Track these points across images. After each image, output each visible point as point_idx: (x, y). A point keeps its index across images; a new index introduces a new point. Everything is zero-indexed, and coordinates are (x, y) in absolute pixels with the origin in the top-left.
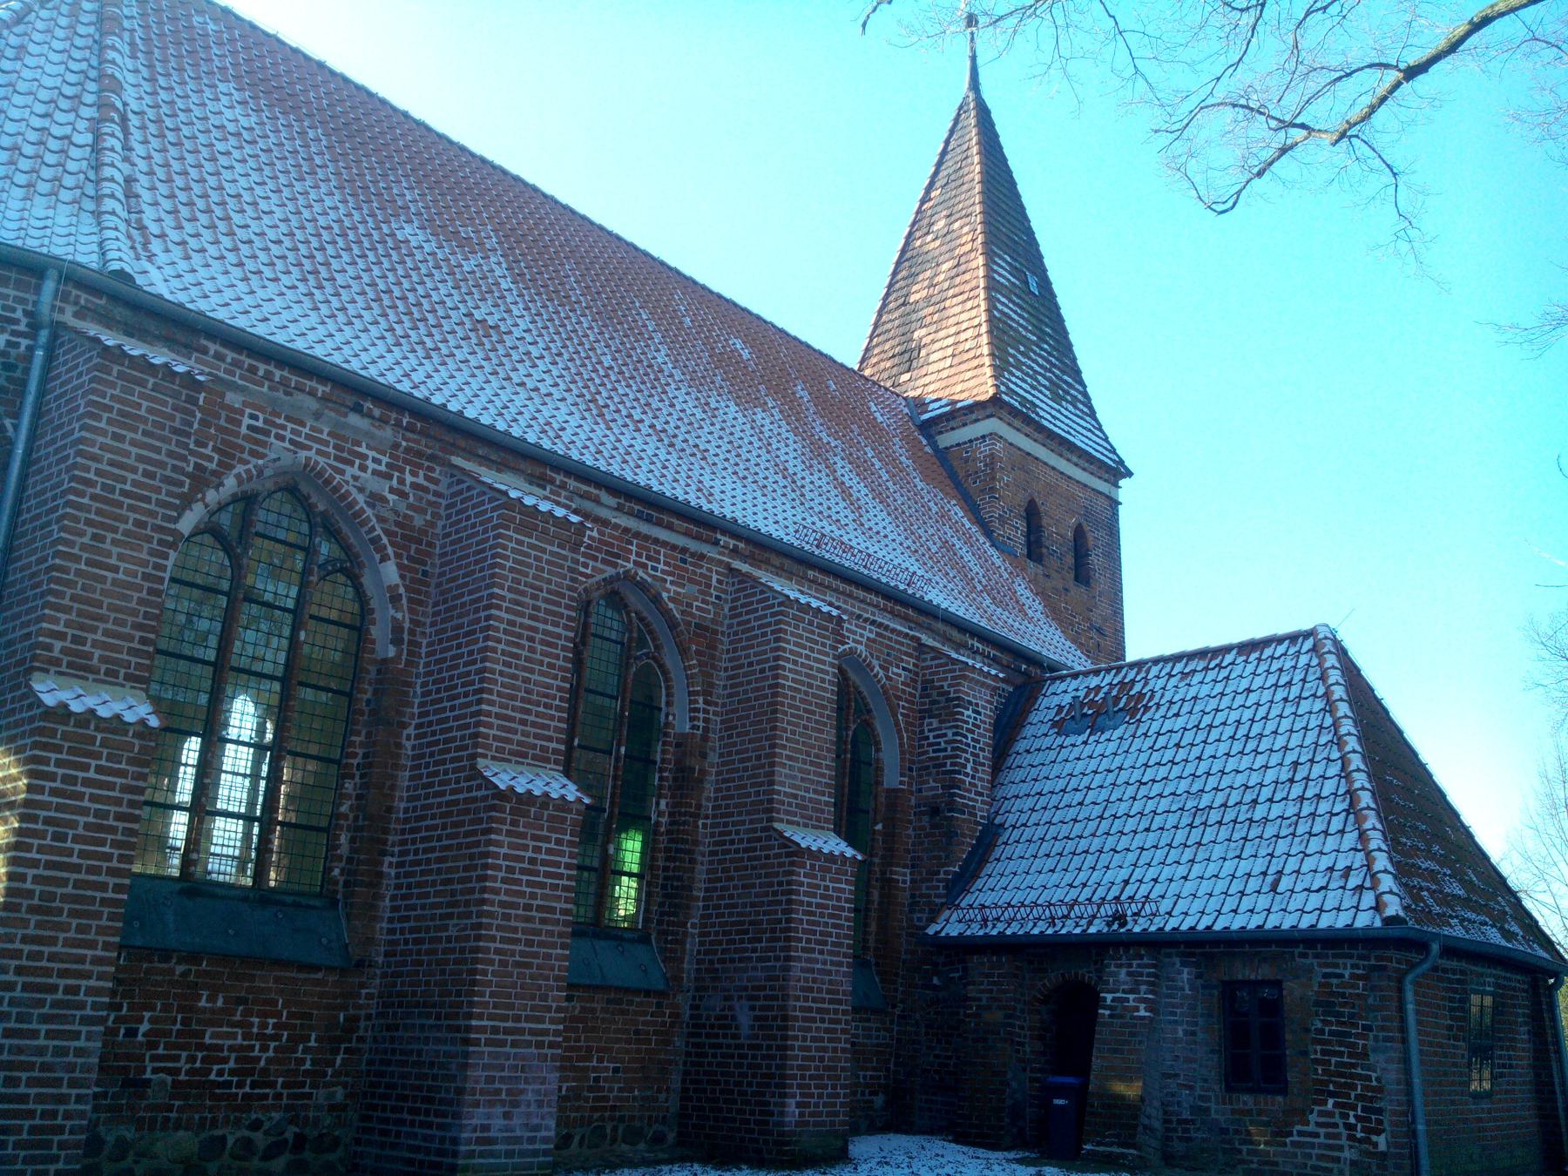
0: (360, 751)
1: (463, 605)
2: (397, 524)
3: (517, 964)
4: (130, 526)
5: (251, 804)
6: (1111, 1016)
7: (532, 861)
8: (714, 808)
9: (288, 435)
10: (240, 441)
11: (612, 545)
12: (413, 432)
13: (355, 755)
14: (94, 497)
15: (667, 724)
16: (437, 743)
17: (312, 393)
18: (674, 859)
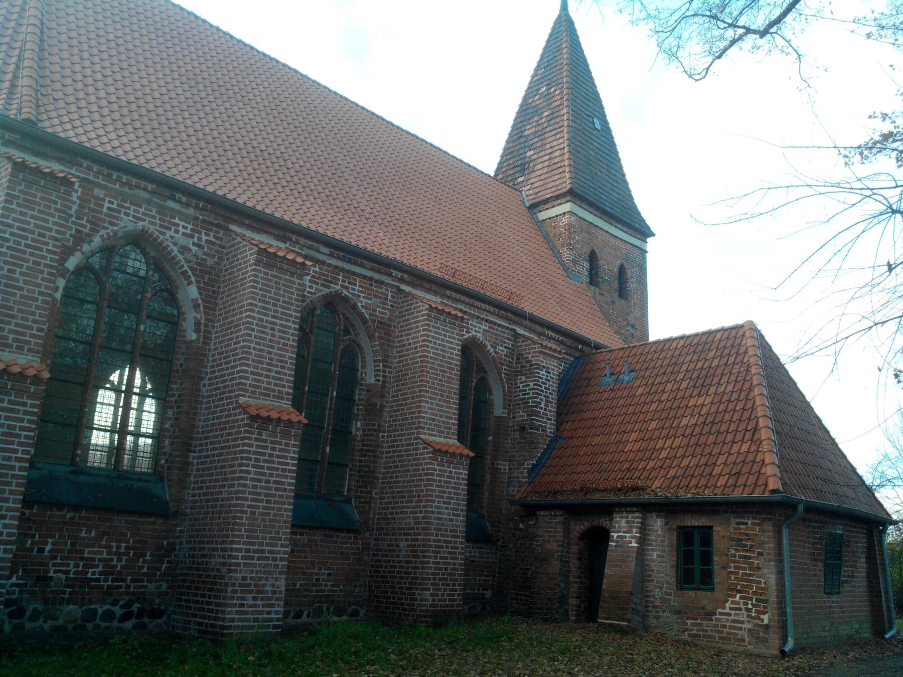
0: (177, 393)
1: (234, 310)
2: (197, 264)
3: (261, 514)
4: (30, 264)
5: (114, 423)
6: (616, 546)
7: (271, 455)
8: (389, 427)
9: (131, 212)
10: (103, 216)
11: (327, 276)
12: (206, 211)
13: (174, 395)
14: (8, 248)
15: (362, 379)
16: (219, 388)
17: (145, 189)
18: (365, 456)
